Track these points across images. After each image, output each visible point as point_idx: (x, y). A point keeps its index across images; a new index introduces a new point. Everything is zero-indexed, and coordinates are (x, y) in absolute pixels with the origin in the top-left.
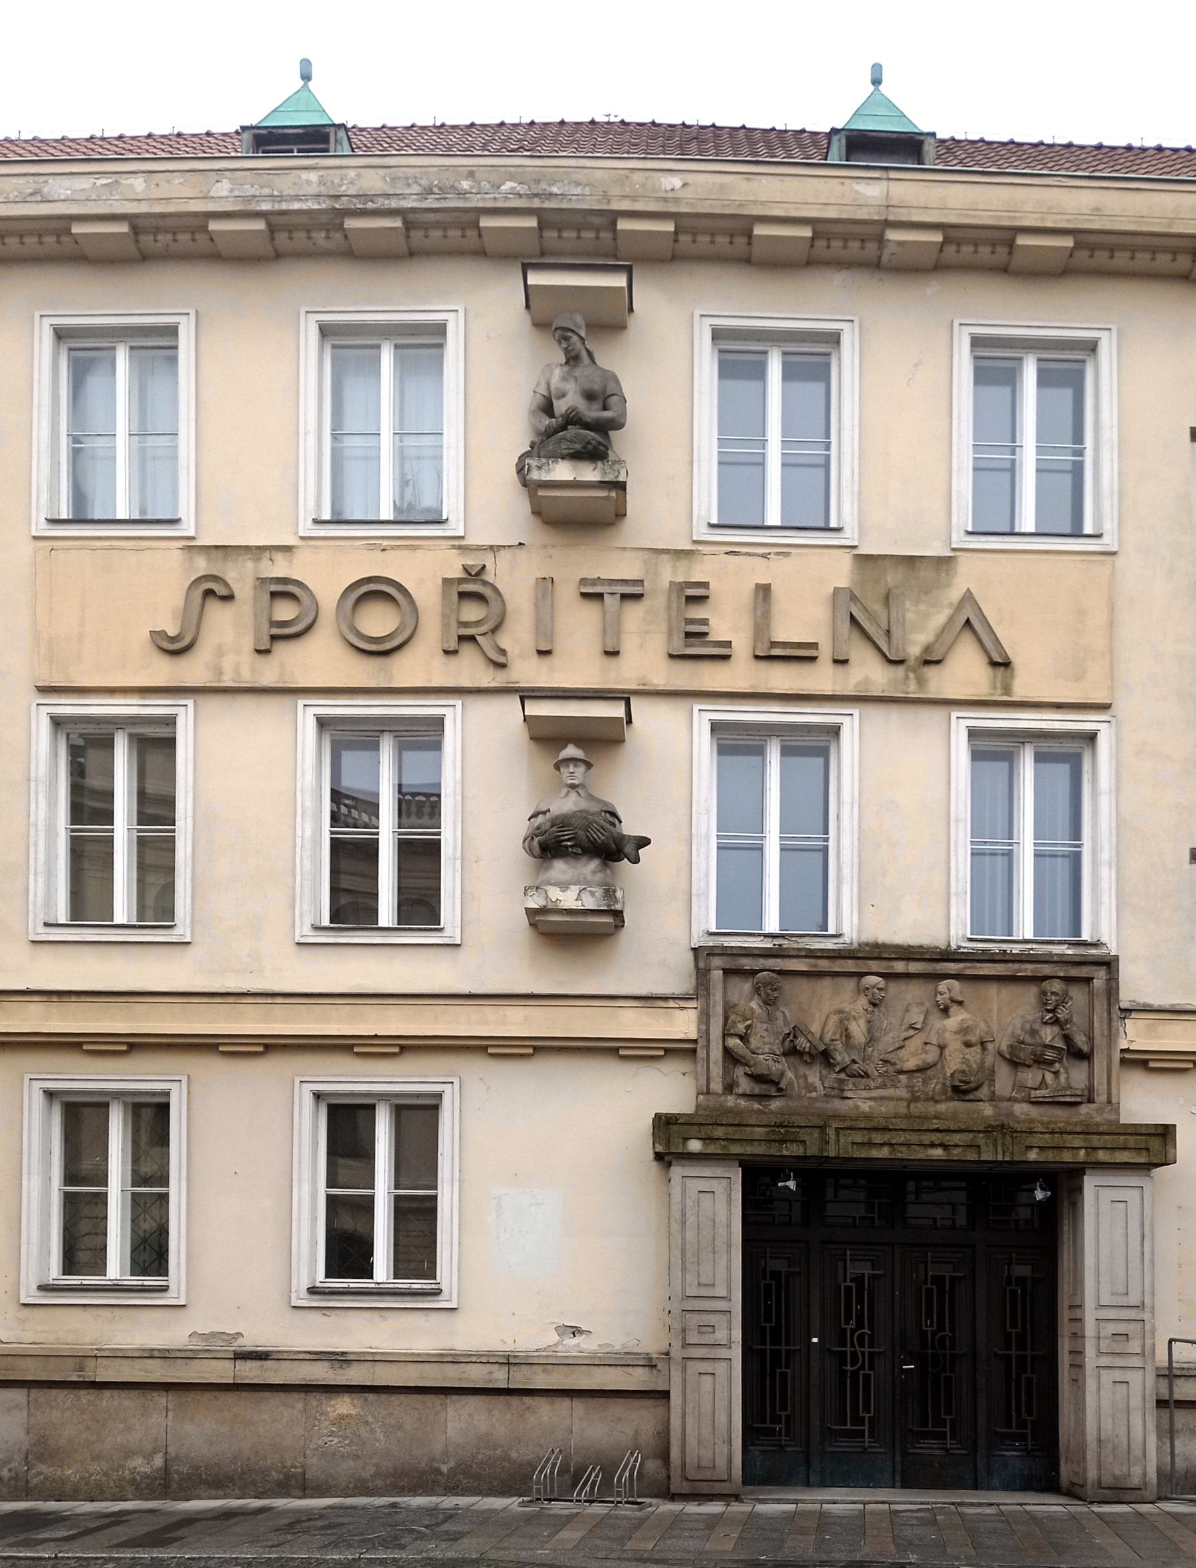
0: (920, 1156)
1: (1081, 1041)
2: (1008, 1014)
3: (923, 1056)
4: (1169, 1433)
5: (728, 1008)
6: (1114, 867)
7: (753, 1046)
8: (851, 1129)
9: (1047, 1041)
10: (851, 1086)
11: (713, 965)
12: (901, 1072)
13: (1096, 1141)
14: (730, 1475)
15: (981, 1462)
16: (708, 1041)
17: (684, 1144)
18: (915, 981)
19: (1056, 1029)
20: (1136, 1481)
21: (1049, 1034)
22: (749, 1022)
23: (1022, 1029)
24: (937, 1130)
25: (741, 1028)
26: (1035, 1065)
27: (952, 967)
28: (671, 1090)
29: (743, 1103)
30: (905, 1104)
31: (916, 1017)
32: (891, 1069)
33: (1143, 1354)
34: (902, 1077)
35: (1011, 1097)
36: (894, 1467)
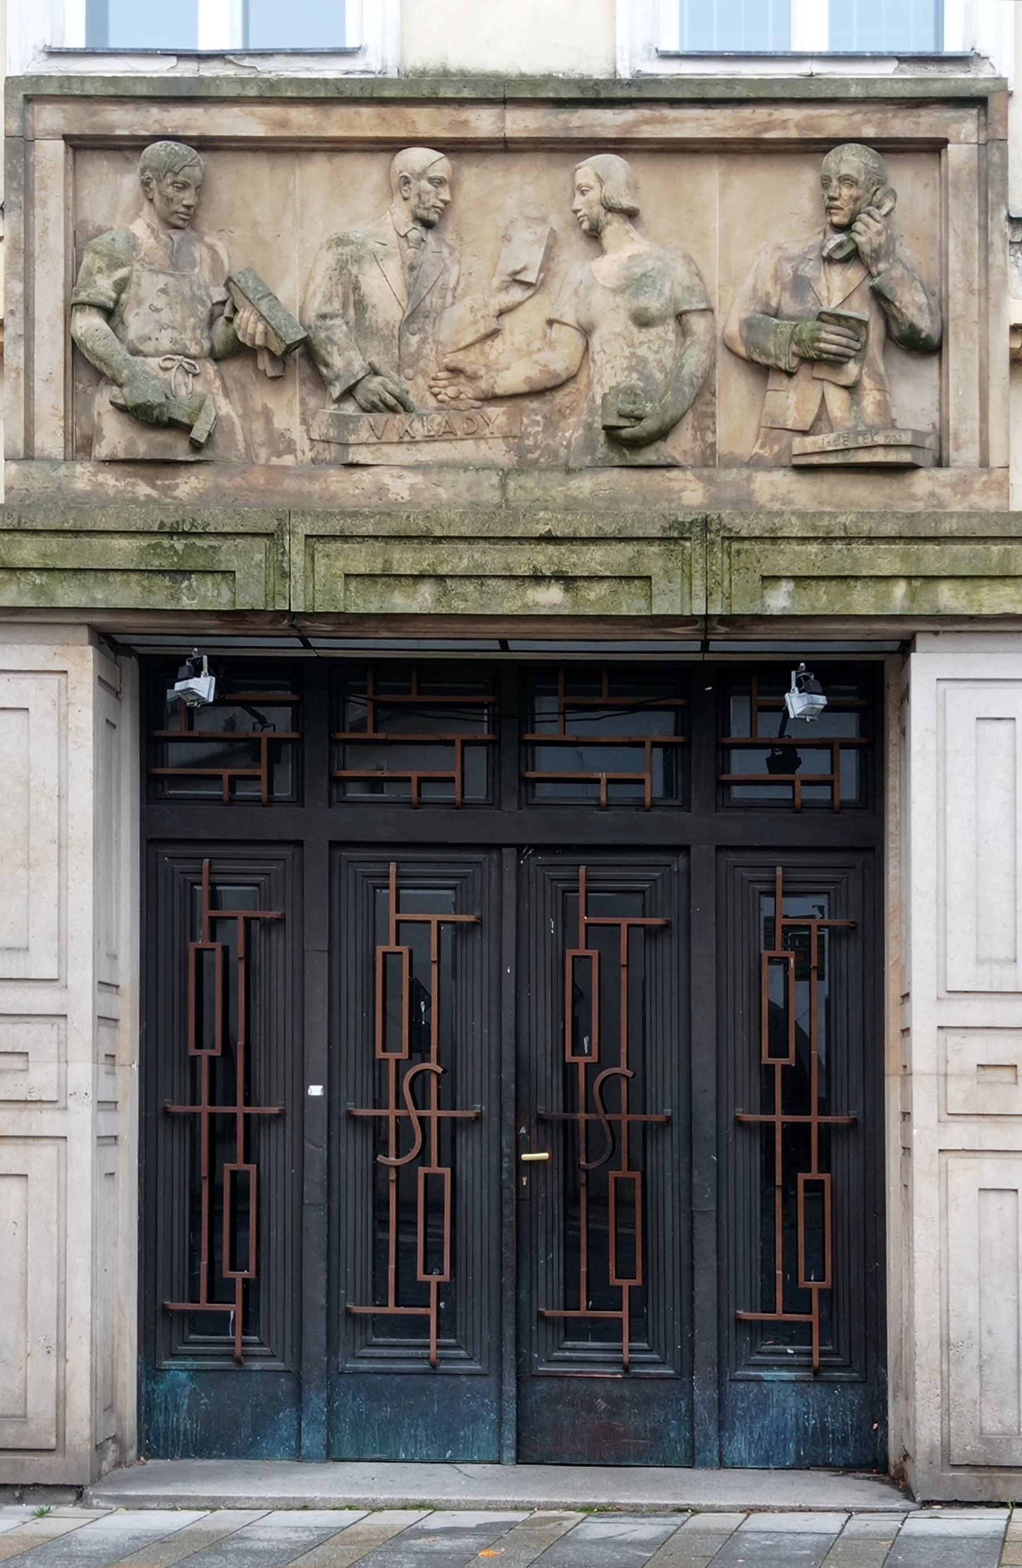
0: (509, 607)
1: (913, 306)
2: (744, 239)
3: (545, 356)
5: (79, 238)
7: (132, 334)
8: (345, 538)
10: (364, 435)
11: (40, 126)
12: (492, 398)
13: (932, 559)
14: (61, 1435)
15: (703, 1394)
16: (29, 321)
19: (854, 274)
21: (837, 289)
23: (776, 278)
24: (548, 539)
25: (104, 287)
26: (804, 371)
27: (608, 122)
29: (110, 481)
30: (495, 480)
31: (526, 254)
32: (468, 391)
34: (496, 413)
36: (500, 1411)
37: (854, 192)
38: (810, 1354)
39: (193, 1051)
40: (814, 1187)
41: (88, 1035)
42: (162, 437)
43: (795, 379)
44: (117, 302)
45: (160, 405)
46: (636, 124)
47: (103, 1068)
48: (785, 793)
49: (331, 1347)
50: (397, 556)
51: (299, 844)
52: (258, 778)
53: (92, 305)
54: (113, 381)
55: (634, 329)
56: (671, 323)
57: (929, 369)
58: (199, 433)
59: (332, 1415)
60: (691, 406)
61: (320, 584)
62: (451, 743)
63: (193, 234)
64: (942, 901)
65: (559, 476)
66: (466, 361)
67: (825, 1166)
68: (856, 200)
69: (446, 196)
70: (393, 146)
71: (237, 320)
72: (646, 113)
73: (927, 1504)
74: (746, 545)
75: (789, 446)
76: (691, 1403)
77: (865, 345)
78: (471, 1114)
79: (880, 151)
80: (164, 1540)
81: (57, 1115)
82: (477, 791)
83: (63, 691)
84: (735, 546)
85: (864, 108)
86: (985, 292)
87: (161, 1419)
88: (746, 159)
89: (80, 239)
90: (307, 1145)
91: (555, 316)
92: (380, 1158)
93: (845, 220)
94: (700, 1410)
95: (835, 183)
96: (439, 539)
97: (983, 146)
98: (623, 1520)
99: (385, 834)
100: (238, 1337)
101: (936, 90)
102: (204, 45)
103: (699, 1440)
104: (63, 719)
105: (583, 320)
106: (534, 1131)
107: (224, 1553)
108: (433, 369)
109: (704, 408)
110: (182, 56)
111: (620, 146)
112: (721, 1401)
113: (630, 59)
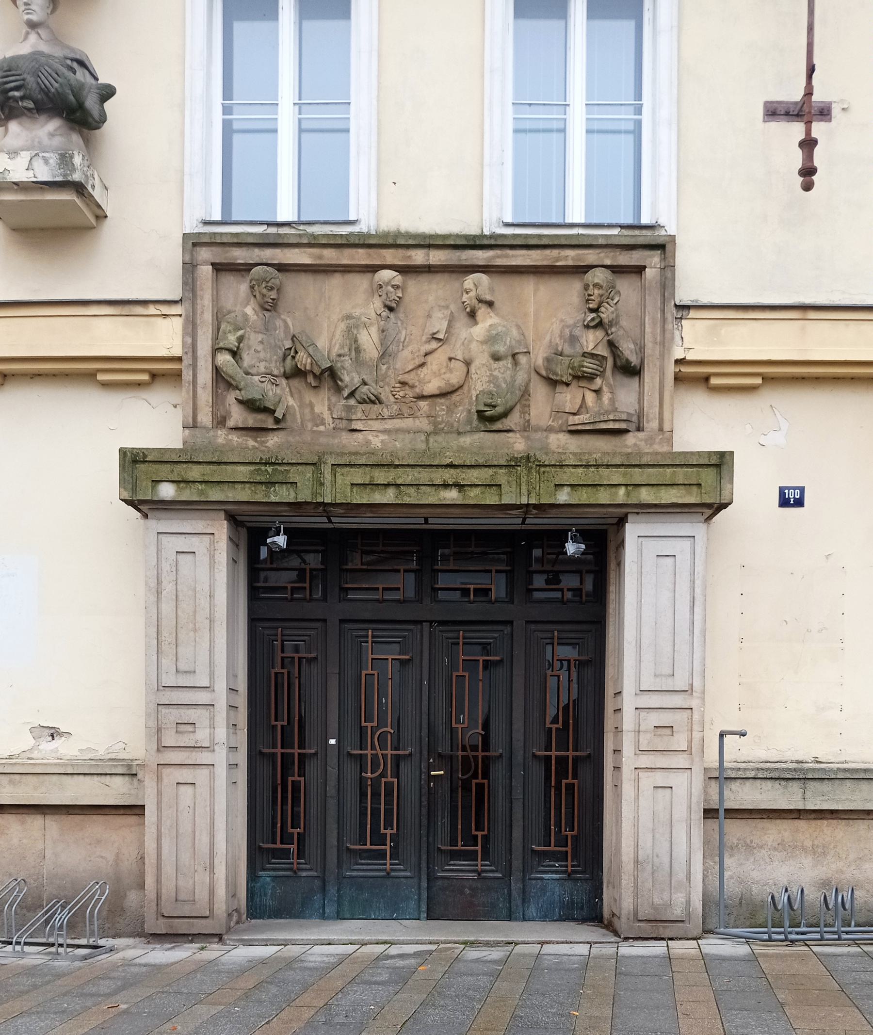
1: (628, 350)
2: (546, 316)
3: (447, 376)
4: (716, 850)
5: (219, 317)
6: (674, 127)
8: (351, 466)
9: (590, 348)
10: (360, 415)
12: (422, 397)
13: (638, 476)
14: (211, 910)
16: (195, 358)
17: (153, 488)
18: (438, 277)
19: (600, 334)
20: (677, 912)
21: (591, 341)
22: (240, 333)
23: (561, 336)
24: (451, 466)
25: (231, 340)
26: (574, 384)
27: (480, 257)
28: (156, 423)
29: (235, 438)
30: (423, 438)
31: (439, 325)
32: (410, 393)
33: (689, 751)
34: (423, 404)
35: (546, 424)
36: (419, 895)
37: (601, 292)
38: (566, 866)
39: (273, 723)
40: (570, 787)
41: (224, 715)
42: (260, 416)
43: (570, 387)
44: (238, 348)
45: (260, 399)
46: (494, 257)
47: (231, 731)
48: (558, 595)
49: (339, 865)
50: (377, 474)
51: (325, 621)
52: (305, 588)
53: (226, 349)
54: (237, 388)
55: (492, 362)
56: (510, 358)
57: (634, 382)
58: (279, 414)
59: (340, 897)
60: (519, 401)
61: (339, 489)
62: (398, 571)
63: (275, 314)
64: (639, 646)
65: (455, 435)
66: (410, 378)
67: (301, 774)
68: (601, 296)
69: (400, 295)
70: (373, 269)
71: (297, 357)
72: (499, 252)
73: (626, 939)
74: (548, 469)
75: (567, 421)
76: (510, 890)
77: (605, 370)
78: (407, 752)
79: (613, 272)
80: (263, 962)
81: (210, 754)
82: (411, 593)
83: (213, 543)
84: (542, 469)
85: (606, 250)
86: (663, 343)
87: (258, 900)
88: (546, 277)
89: (219, 316)
90: (328, 768)
91: (452, 356)
92: (363, 774)
93: (596, 306)
94: (514, 893)
95: (591, 287)
96: (397, 466)
97: (663, 269)
98: (483, 948)
99: (367, 616)
100: (295, 861)
101: (641, 241)
102: (280, 218)
103: (514, 908)
104: (212, 557)
105: (466, 357)
106: (437, 762)
107: (294, 969)
108: (393, 382)
109: (524, 402)
110: (269, 224)
111: (485, 269)
112: (524, 889)
113: (491, 227)
